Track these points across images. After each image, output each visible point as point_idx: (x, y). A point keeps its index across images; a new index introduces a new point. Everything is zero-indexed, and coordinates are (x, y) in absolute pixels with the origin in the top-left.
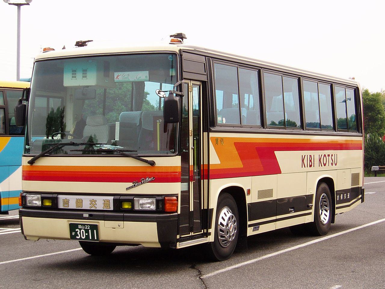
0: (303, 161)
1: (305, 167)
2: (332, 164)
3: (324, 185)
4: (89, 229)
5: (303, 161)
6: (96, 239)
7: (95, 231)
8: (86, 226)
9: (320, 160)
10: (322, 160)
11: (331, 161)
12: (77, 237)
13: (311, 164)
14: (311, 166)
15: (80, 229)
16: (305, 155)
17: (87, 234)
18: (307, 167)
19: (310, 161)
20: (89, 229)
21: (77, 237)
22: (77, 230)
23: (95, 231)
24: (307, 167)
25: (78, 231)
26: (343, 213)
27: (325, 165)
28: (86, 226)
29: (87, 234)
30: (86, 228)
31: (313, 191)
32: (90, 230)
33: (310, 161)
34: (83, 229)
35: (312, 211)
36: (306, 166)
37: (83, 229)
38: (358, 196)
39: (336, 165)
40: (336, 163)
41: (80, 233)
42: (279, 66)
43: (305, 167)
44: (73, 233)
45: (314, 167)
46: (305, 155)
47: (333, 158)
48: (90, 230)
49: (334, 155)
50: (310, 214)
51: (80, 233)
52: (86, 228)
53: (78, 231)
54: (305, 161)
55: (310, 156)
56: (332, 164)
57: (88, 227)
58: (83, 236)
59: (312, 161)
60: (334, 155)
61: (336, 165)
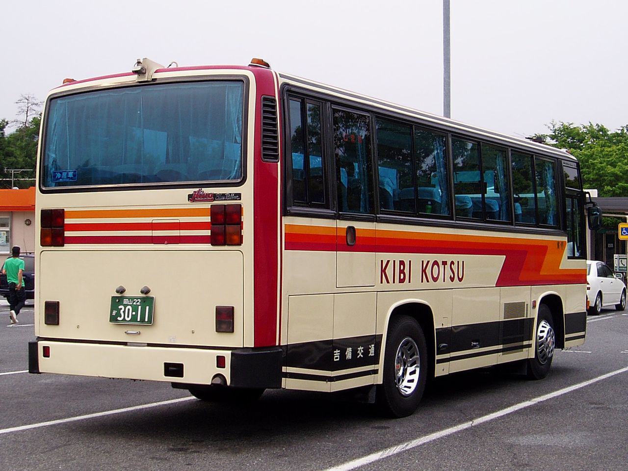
0: (383, 271)
1: (388, 282)
2: (452, 279)
3: (408, 321)
4: (140, 305)
5: (383, 271)
6: (146, 320)
7: (147, 307)
8: (135, 301)
9: (424, 271)
10: (428, 271)
11: (449, 273)
12: (119, 318)
13: (402, 278)
14: (402, 281)
15: (125, 306)
16: (388, 261)
17: (134, 313)
18: (394, 282)
19: (402, 271)
20: (140, 305)
21: (119, 318)
22: (120, 307)
23: (147, 307)
24: (394, 282)
25: (121, 309)
26: (573, 350)
27: (435, 280)
28: (135, 301)
29: (134, 313)
30: (134, 304)
31: (384, 331)
32: (140, 307)
33: (402, 271)
34: (129, 305)
35: (380, 367)
36: (391, 280)
37: (129, 305)
38: (523, 341)
39: (460, 280)
40: (460, 277)
41: (124, 312)
42: (393, 108)
43: (388, 282)
44: (114, 313)
45: (409, 282)
46: (388, 261)
47: (455, 267)
48: (140, 307)
49: (397, 279)
50: (375, 372)
51: (124, 312)
52: (134, 304)
53: (121, 309)
54: (390, 271)
55: (402, 263)
56: (452, 279)
57: (138, 302)
58: (128, 317)
59: (407, 271)
60: (456, 264)
61: (452, 281)
